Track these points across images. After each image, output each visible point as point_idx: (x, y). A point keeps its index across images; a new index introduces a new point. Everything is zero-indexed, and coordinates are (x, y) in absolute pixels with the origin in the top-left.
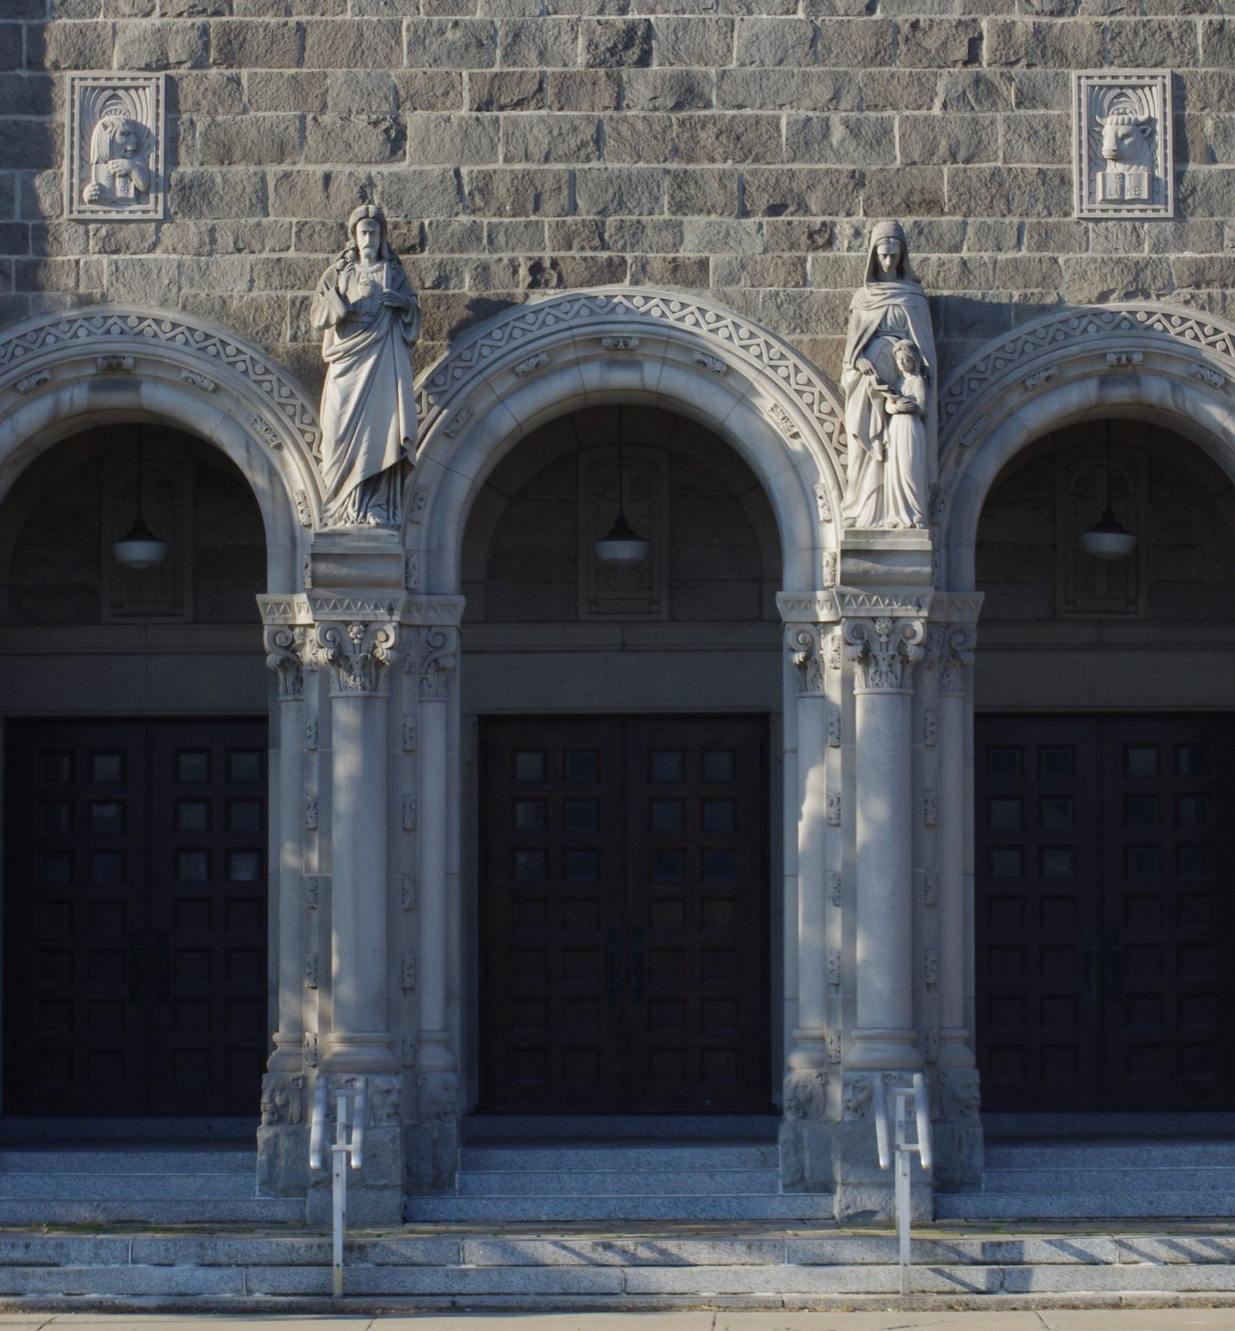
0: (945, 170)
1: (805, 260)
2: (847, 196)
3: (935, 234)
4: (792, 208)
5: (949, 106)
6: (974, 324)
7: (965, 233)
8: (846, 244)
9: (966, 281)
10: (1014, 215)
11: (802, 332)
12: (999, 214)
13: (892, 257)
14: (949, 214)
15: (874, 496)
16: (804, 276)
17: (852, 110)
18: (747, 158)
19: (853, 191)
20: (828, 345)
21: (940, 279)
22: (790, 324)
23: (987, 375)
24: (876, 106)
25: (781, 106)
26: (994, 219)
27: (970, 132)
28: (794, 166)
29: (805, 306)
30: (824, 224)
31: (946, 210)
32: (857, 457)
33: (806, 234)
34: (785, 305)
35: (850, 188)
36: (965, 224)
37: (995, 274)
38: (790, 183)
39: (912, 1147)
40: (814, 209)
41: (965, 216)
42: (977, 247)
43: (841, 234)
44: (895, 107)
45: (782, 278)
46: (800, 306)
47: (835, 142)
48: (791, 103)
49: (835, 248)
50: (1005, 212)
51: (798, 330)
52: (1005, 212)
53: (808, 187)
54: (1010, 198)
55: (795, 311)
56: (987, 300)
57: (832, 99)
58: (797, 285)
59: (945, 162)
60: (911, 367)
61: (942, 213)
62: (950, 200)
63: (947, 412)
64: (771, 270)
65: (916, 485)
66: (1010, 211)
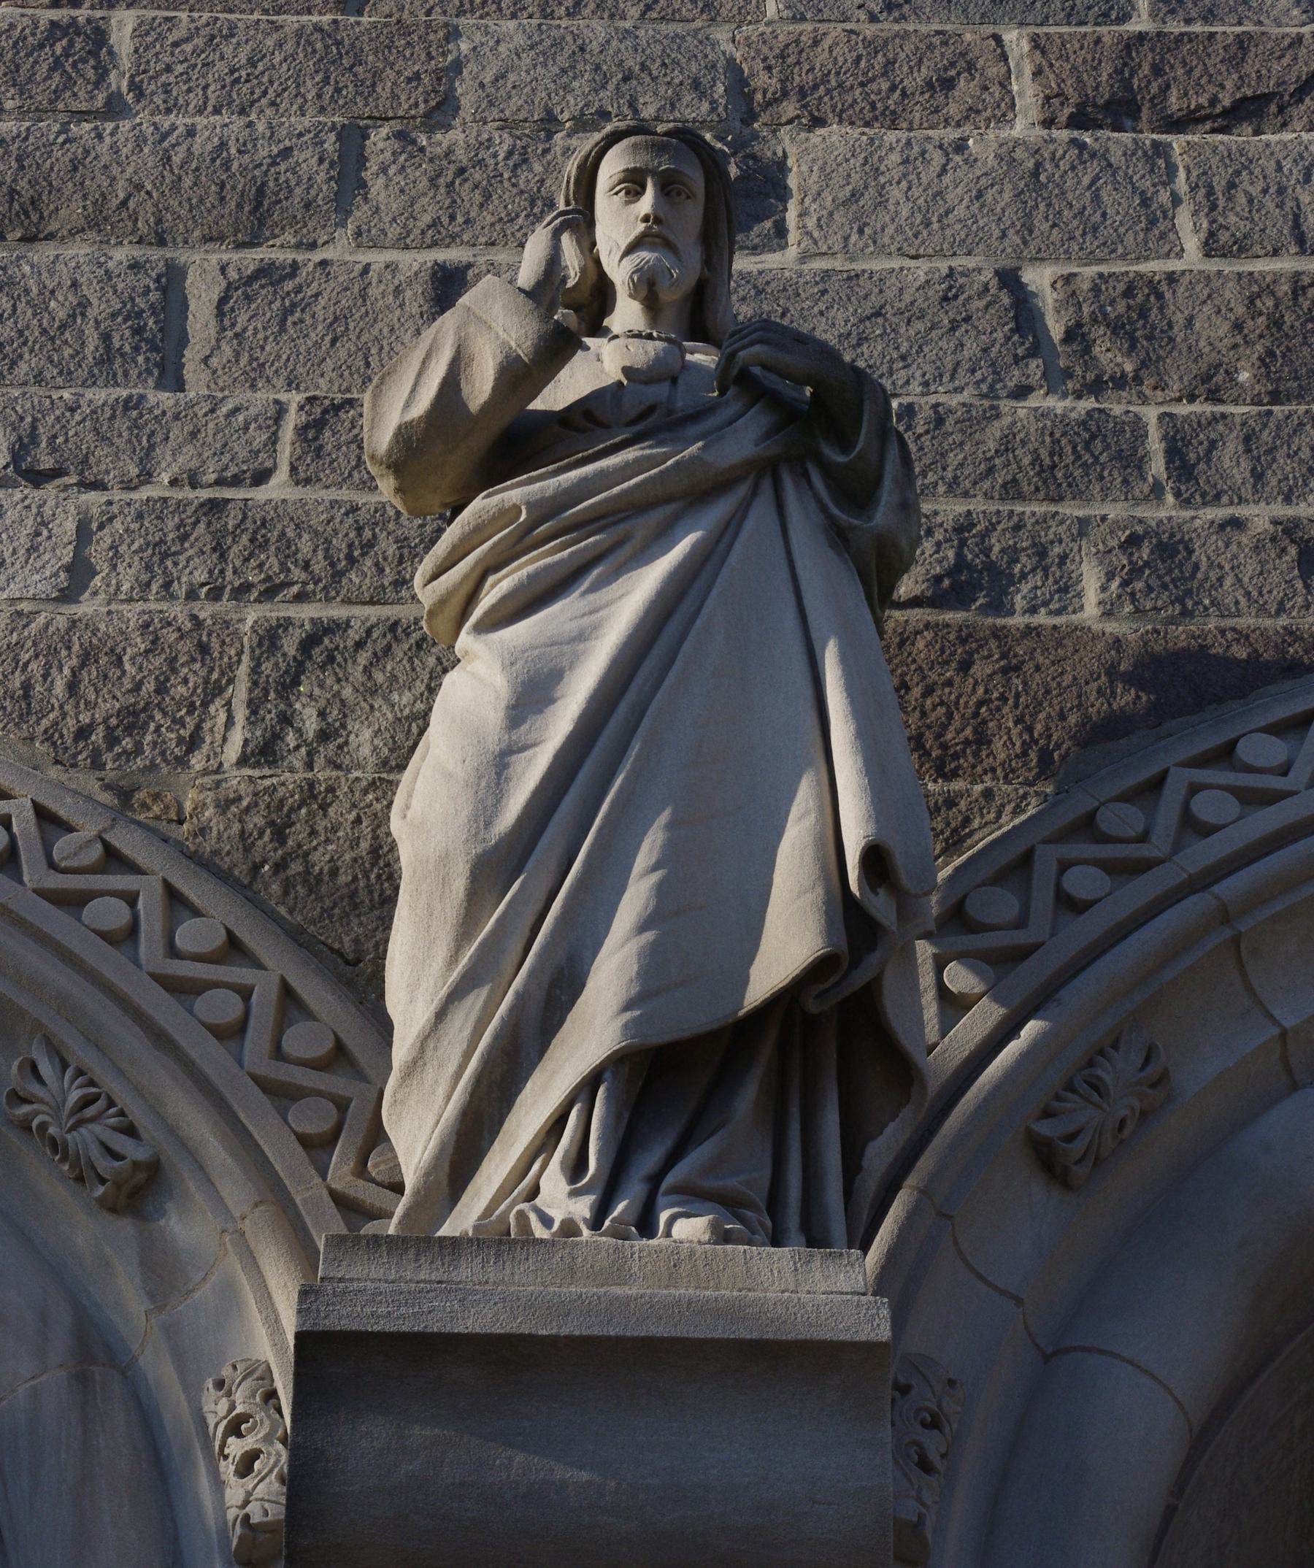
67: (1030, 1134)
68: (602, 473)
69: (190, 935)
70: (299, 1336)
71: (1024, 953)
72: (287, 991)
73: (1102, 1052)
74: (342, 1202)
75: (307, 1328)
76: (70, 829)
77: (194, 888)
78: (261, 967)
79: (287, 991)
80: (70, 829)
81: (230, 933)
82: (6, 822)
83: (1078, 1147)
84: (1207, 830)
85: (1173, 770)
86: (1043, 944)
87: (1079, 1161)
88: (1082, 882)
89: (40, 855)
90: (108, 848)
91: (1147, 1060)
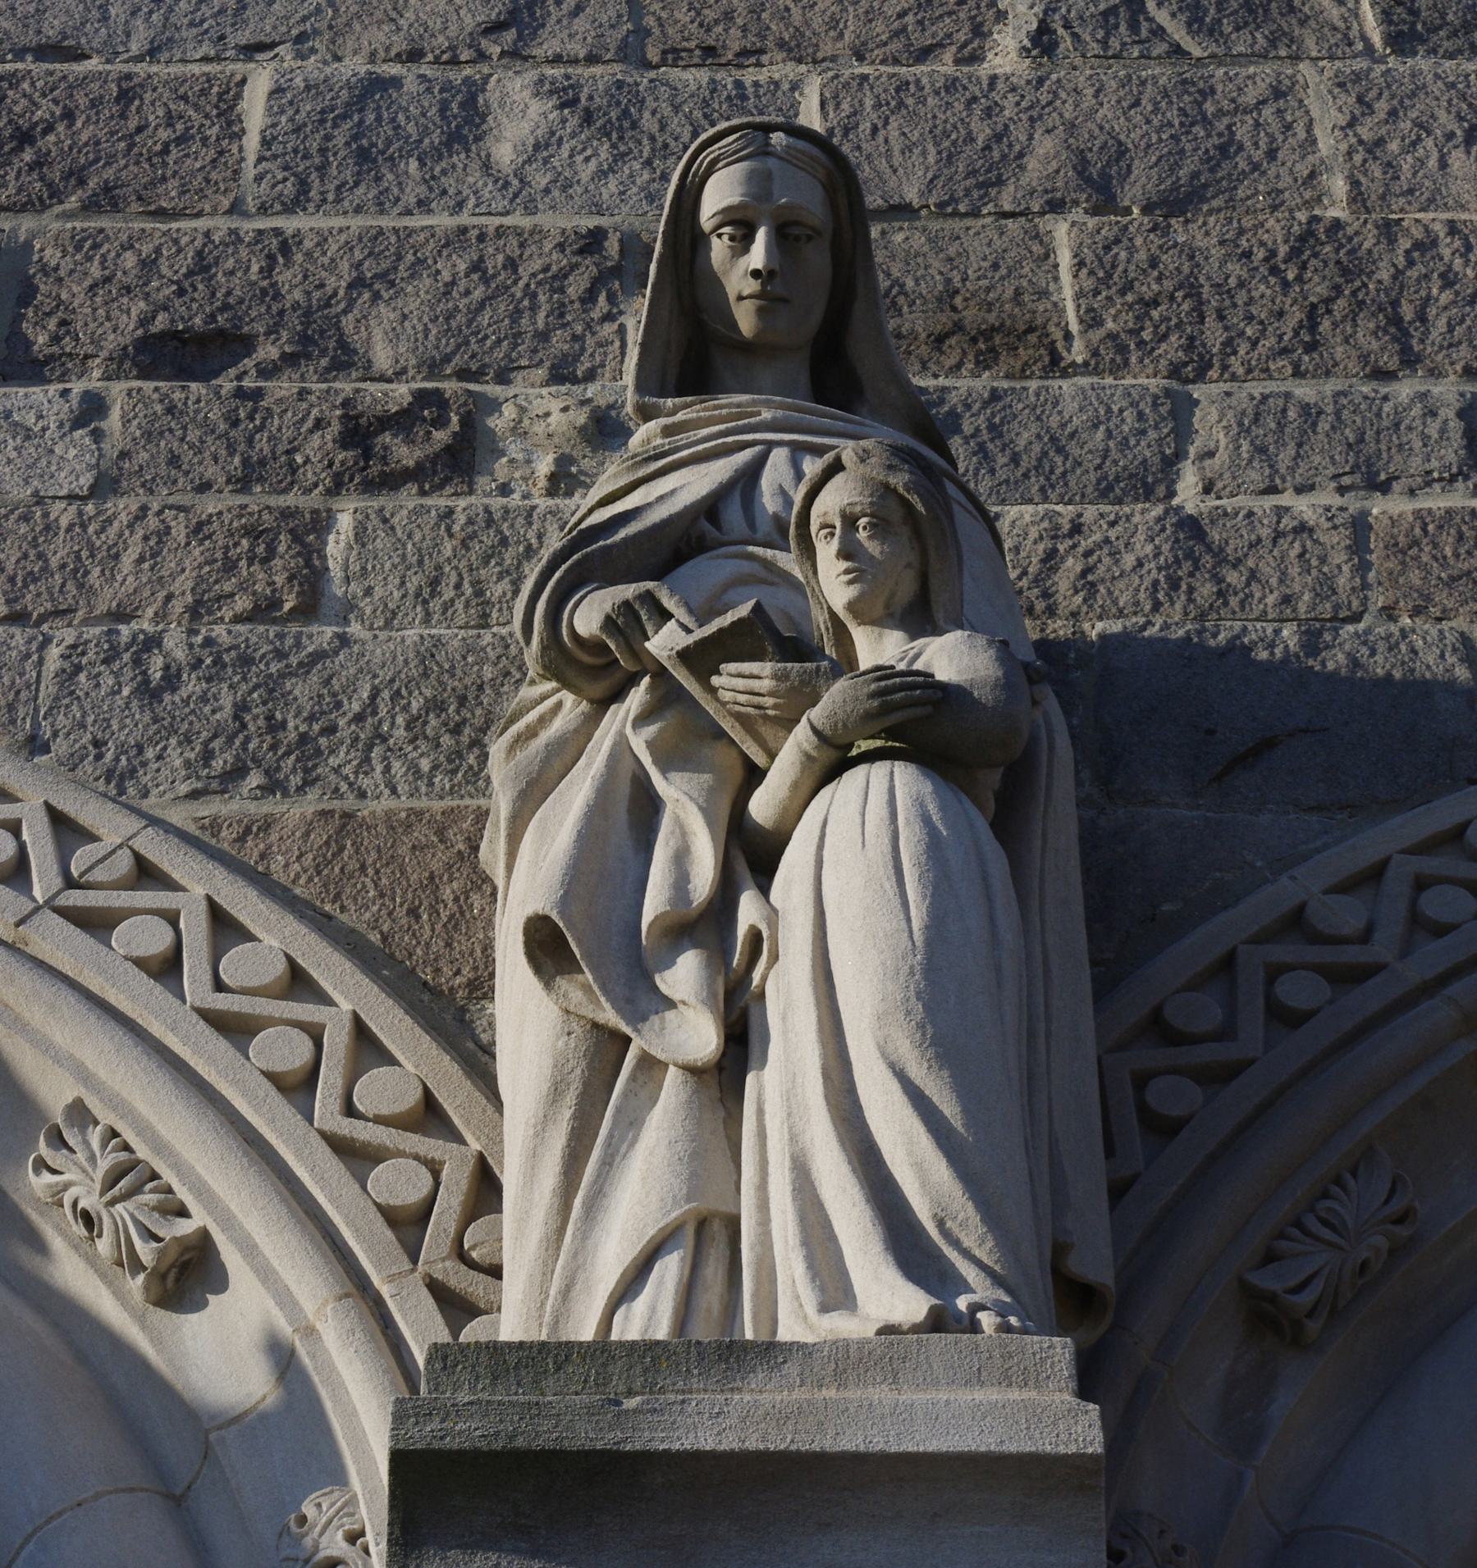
0: (1062, 234)
1: (322, 523)
2: (560, 311)
3: (1024, 436)
4: (268, 351)
5: (1066, 43)
6: (1267, 745)
7: (1183, 432)
8: (544, 466)
9: (1206, 590)
10: (1435, 373)
11: (273, 786)
12: (1353, 366)
13: (785, 236)
14: (1085, 368)
15: (669, 1270)
16: (311, 579)
17: (592, 59)
18: (57, 195)
19: (589, 297)
20: (421, 833)
21: (1063, 582)
22: (207, 756)
23: (1381, 949)
24: (709, 51)
25: (251, 50)
26: (1330, 386)
27: (1173, 115)
28: (290, 224)
29: (302, 690)
30: (421, 397)
31: (1078, 353)
32: (556, 1092)
33: (335, 428)
34: (191, 685)
35: (576, 286)
36: (1180, 411)
37: (1363, 567)
38: (268, 271)
39: (158, 234)
40: (382, 358)
41: (1175, 372)
42: (1256, 476)
43: (522, 434)
44: (797, 50)
45: (183, 584)
46: (272, 687)
47: (504, 154)
48: (301, 38)
49: (483, 482)
50: (1388, 360)
51: (254, 779)
52: (1388, 360)
53: (358, 283)
54: (1407, 311)
55: (241, 708)
56: (1335, 660)
57: (494, 28)
58: (264, 611)
59: (1056, 206)
60: (906, 588)
61: (1055, 365)
62: (1092, 320)
63: (1143, 1109)
64: (127, 560)
65: (963, 1089)
66: (1410, 360)
67: (1247, 1290)
68: (755, 1295)
69: (238, 965)
70: (398, 1459)
71: (1233, 1071)
72: (361, 1031)
73: (1338, 1181)
74: (440, 1292)
75: (401, 1446)
76: (94, 838)
77: (245, 904)
78: (329, 1002)
79: (361, 1031)
80: (94, 838)
81: (291, 961)
82: (14, 828)
83: (1306, 1298)
84: (1441, 930)
85: (1397, 858)
86: (1252, 1062)
87: (1310, 1314)
88: (1299, 991)
89: (54, 869)
90: (139, 859)
91: (1392, 1192)
